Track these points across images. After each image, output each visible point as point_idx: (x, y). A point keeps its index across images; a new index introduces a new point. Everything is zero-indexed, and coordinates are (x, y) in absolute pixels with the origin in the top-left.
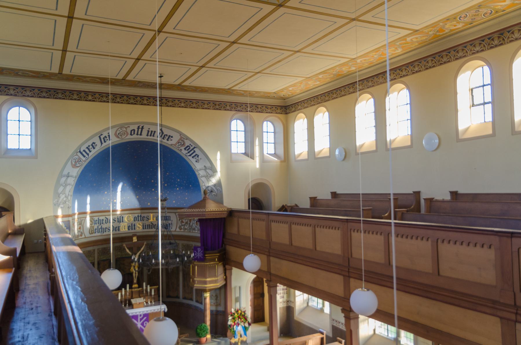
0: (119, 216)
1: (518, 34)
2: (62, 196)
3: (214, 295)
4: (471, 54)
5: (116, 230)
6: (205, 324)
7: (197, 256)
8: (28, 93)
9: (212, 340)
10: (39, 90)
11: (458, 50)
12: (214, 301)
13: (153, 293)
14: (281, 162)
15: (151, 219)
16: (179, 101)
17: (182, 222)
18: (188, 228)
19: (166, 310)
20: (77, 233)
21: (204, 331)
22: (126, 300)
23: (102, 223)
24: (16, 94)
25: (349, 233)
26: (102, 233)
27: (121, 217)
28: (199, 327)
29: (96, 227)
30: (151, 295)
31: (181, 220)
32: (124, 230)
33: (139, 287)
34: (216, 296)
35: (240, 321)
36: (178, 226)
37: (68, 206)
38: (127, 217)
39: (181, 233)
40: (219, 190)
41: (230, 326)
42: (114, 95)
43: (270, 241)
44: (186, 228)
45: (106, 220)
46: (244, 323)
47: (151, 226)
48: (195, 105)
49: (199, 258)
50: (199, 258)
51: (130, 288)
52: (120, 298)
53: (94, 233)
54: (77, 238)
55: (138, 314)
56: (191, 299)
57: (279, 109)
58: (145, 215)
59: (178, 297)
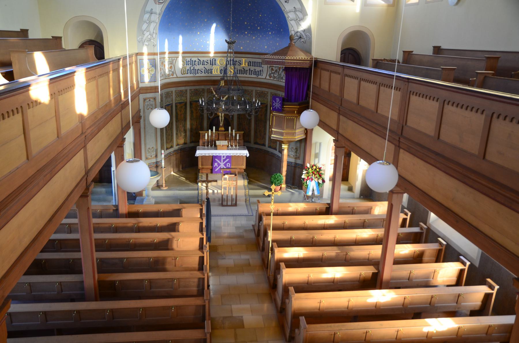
0: (212, 58)
2: (147, 34)
3: (294, 148)
5: (209, 73)
6: (280, 175)
7: (275, 106)
9: (286, 190)
12: (293, 154)
13: (238, 138)
14: (389, 6)
15: (243, 65)
17: (272, 69)
18: (277, 76)
19: (248, 155)
20: (168, 72)
21: (277, 181)
22: (212, 141)
23: (195, 65)
25: (408, 96)
26: (195, 74)
27: (214, 60)
28: (273, 176)
29: (188, 67)
30: (236, 139)
31: (271, 68)
32: (217, 73)
33: (225, 131)
34: (296, 149)
35: (314, 177)
36: (268, 74)
37: (153, 45)
38: (219, 60)
39: (270, 82)
40: (308, 36)
41: (304, 179)
43: (342, 97)
44: (275, 77)
45: (198, 62)
46: (318, 179)
47: (243, 71)
49: (277, 108)
50: (277, 108)
51: (216, 131)
52: (206, 138)
53: (186, 74)
54: (168, 77)
55: (221, 155)
56: (275, 149)
58: (238, 59)
59: (264, 145)
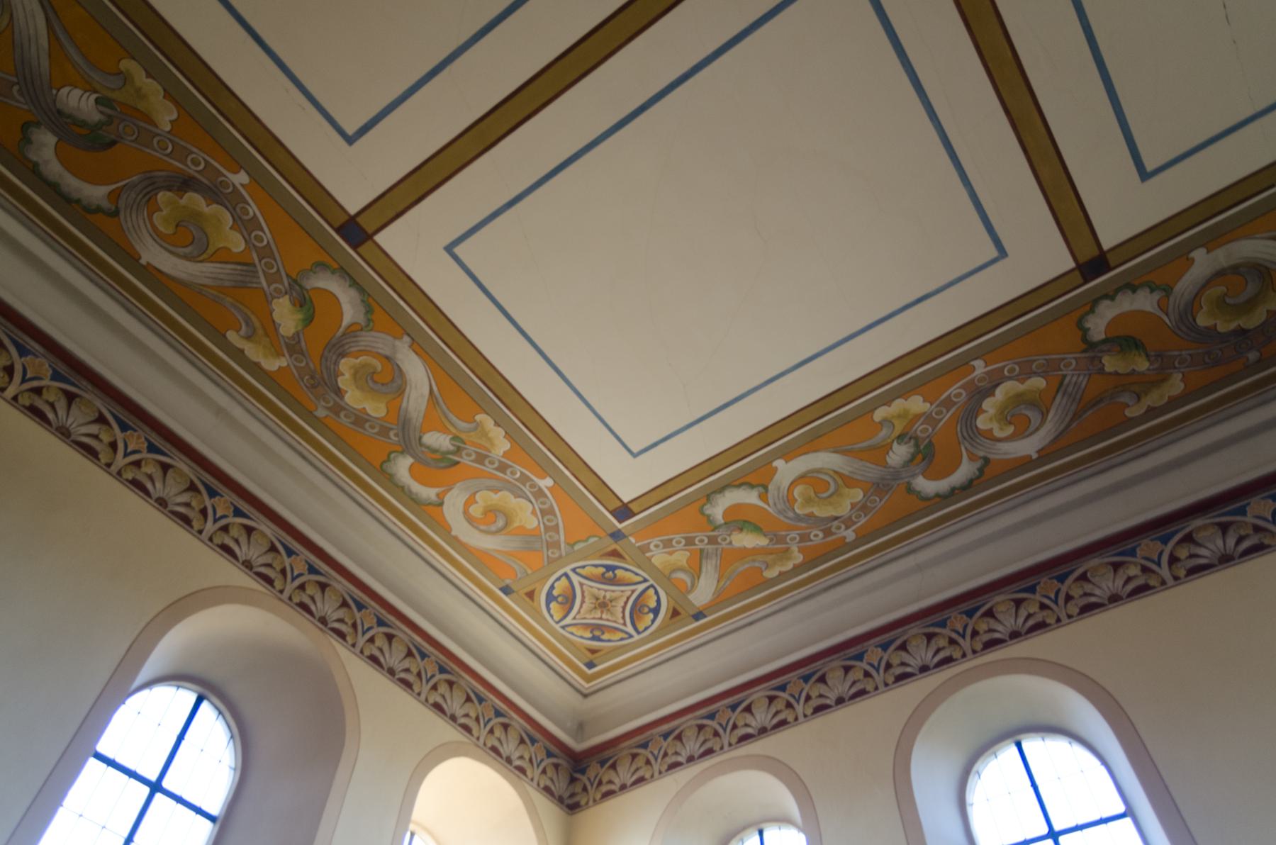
1: (695, 744)
4: (663, 770)
8: (171, 489)
11: (681, 732)
19: (848, 540)
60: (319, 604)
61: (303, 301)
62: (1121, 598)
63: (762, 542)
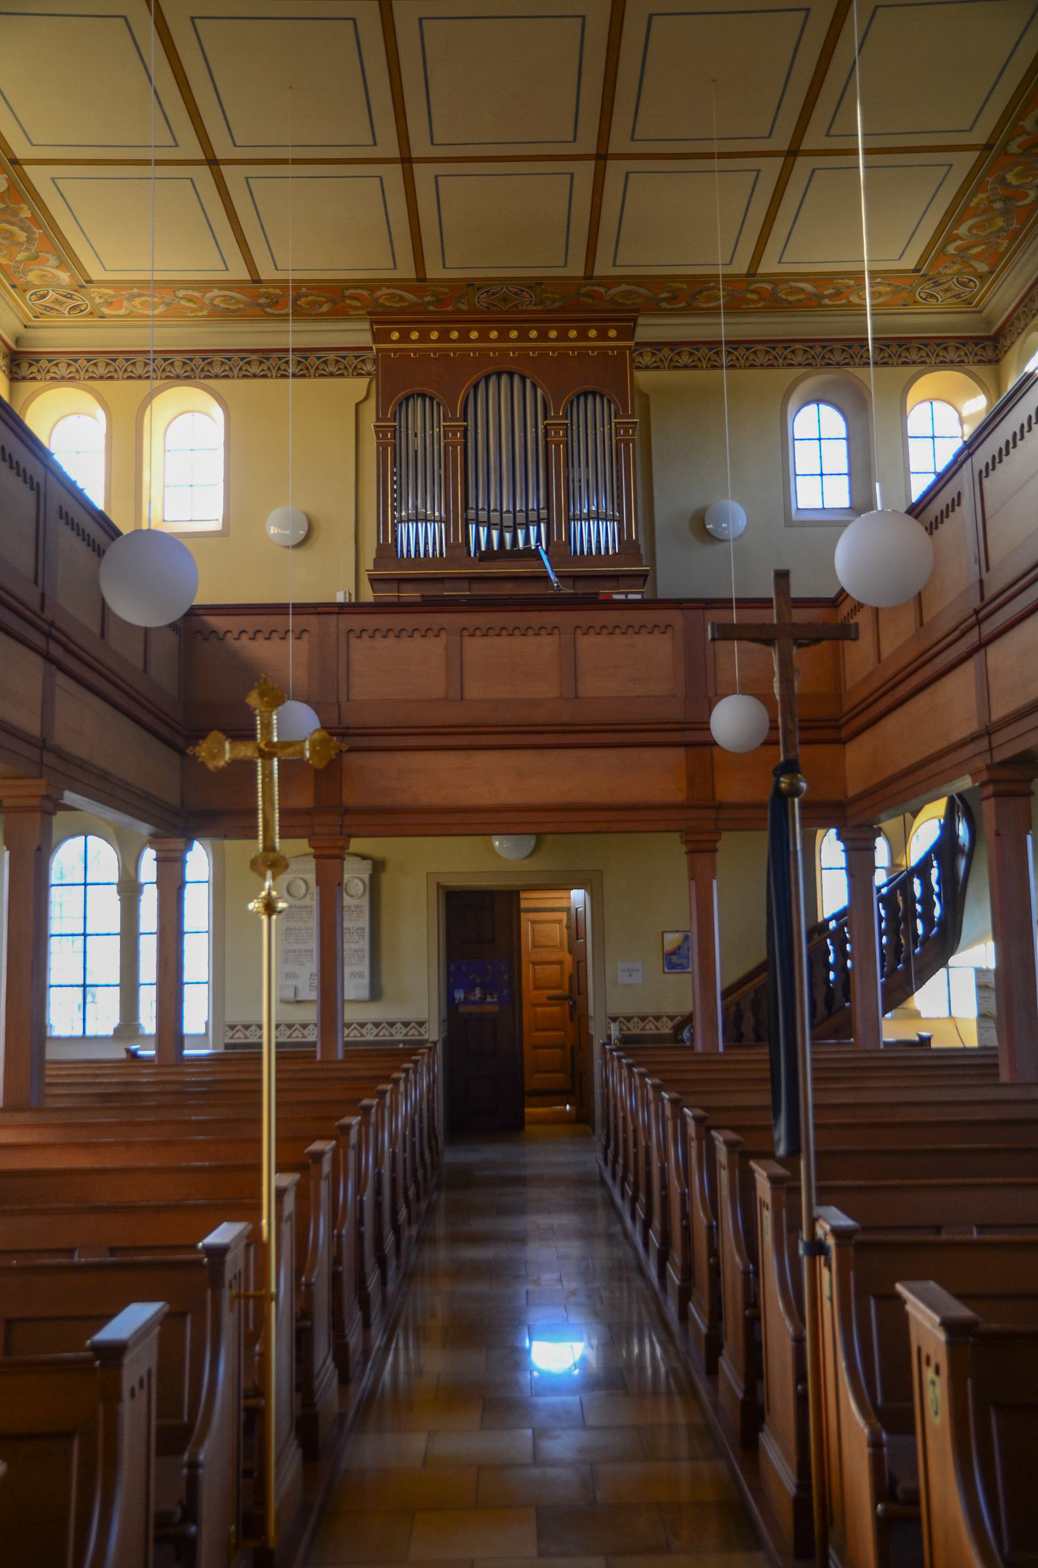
8: (762, 359)
10: (127, 360)
16: (827, 347)
24: (810, 361)
42: (734, 344)
48: (257, 367)
57: (63, 366)
60: (833, 359)
61: (753, 292)
62: (26, 379)
63: (984, 247)
